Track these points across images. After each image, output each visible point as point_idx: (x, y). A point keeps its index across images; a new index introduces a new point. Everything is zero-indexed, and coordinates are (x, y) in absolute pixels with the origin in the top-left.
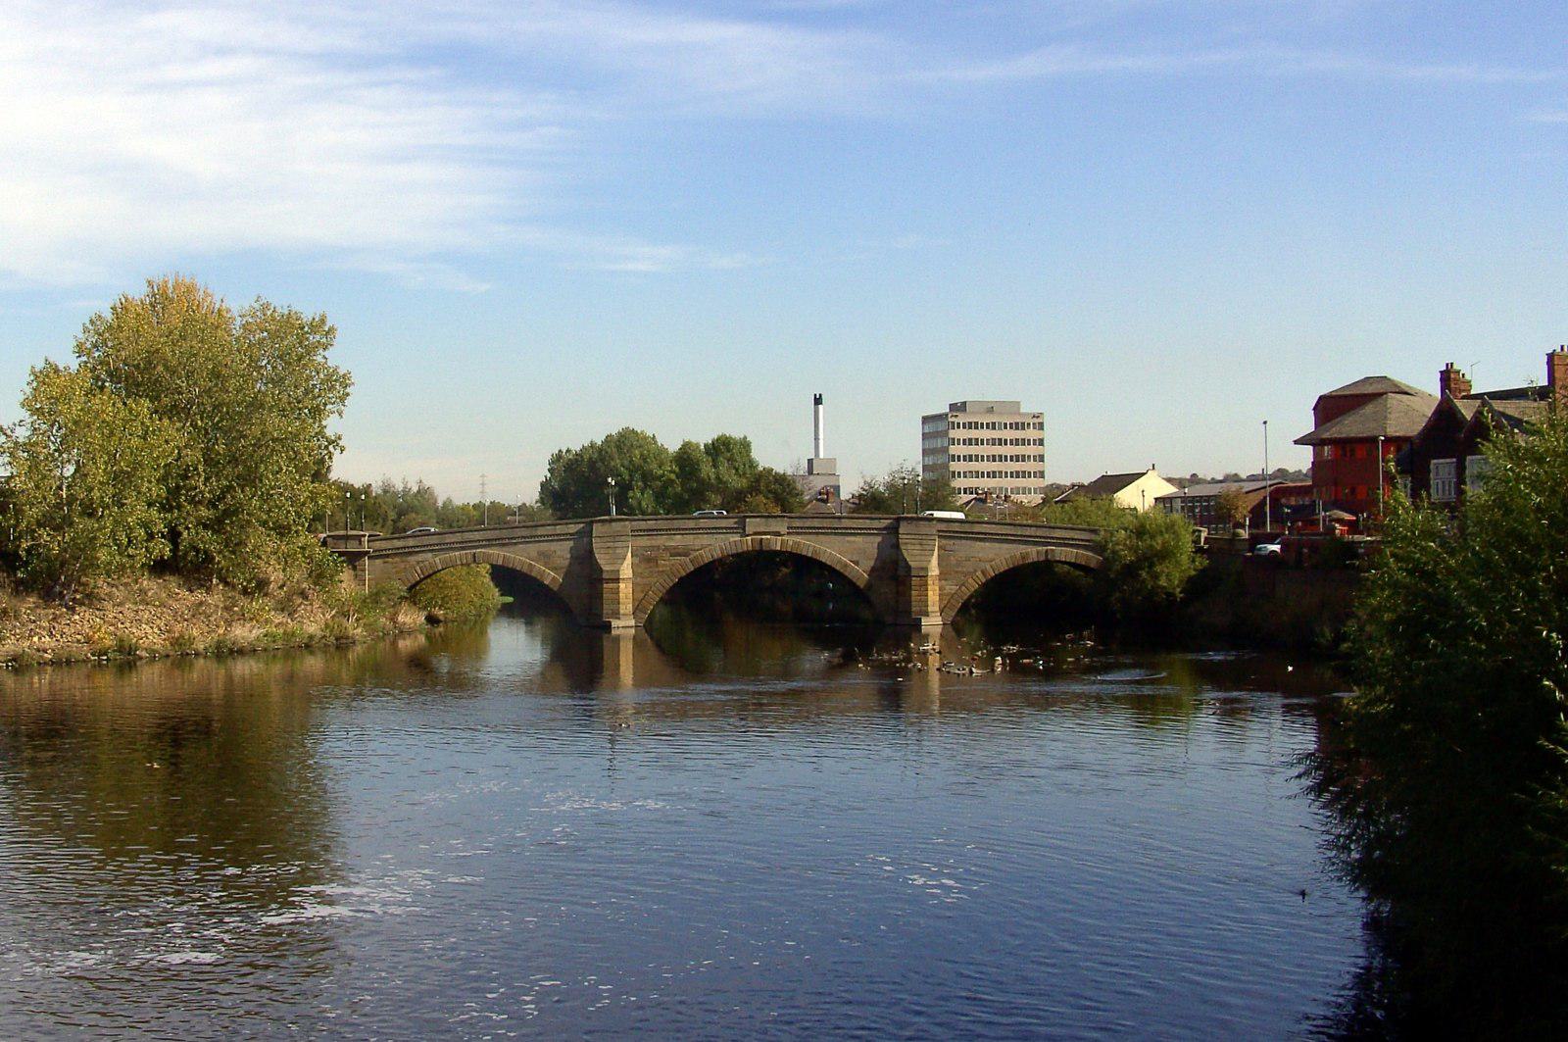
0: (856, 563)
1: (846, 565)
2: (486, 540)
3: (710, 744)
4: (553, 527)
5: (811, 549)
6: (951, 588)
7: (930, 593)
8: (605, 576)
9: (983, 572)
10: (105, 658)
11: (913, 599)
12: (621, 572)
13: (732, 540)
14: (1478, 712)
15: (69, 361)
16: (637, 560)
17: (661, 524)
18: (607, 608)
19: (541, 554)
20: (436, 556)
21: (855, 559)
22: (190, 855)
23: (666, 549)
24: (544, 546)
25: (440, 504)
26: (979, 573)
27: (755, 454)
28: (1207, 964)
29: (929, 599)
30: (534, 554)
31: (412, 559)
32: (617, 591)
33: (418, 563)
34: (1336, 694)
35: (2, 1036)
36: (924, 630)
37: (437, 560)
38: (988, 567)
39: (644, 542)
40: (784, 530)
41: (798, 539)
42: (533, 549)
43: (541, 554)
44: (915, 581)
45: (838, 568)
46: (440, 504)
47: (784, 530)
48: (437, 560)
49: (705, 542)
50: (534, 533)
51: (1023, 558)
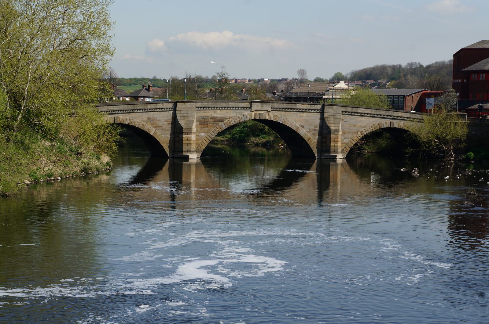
0: (303, 127)
1: (298, 128)
3: (444, 201)
5: (282, 119)
6: (346, 141)
8: (184, 131)
9: (361, 133)
10: (53, 178)
11: (331, 145)
13: (244, 113)
14: (475, 178)
15: (425, 66)
16: (198, 123)
17: (210, 104)
18: (185, 148)
19: (149, 119)
22: (160, 234)
23: (213, 118)
24: (151, 115)
26: (359, 133)
28: (229, 238)
30: (145, 119)
32: (189, 139)
35: (488, 248)
38: (364, 130)
39: (202, 113)
40: (270, 109)
41: (276, 113)
42: (145, 116)
43: (149, 119)
44: (333, 136)
45: (294, 129)
47: (270, 109)
49: (232, 115)
50: (146, 107)
51: (379, 126)
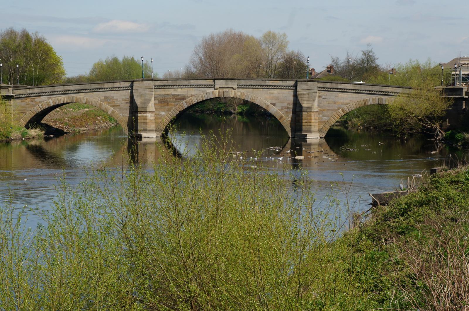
0: (274, 105)
1: (268, 106)
2: (118, 88)
4: (166, 81)
7: (313, 121)
8: (139, 110)
9: (343, 110)
12: (148, 108)
20: (50, 98)
21: (274, 102)
24: (108, 94)
25: (104, 63)
26: (340, 111)
27: (57, 54)
29: (312, 124)
31: (37, 100)
33: (40, 102)
34: (434, 168)
36: (309, 141)
37: (50, 101)
38: (345, 108)
39: (161, 92)
40: (235, 86)
42: (102, 95)
44: (304, 114)
46: (104, 63)
47: (235, 86)
48: (50, 101)
50: (102, 87)
